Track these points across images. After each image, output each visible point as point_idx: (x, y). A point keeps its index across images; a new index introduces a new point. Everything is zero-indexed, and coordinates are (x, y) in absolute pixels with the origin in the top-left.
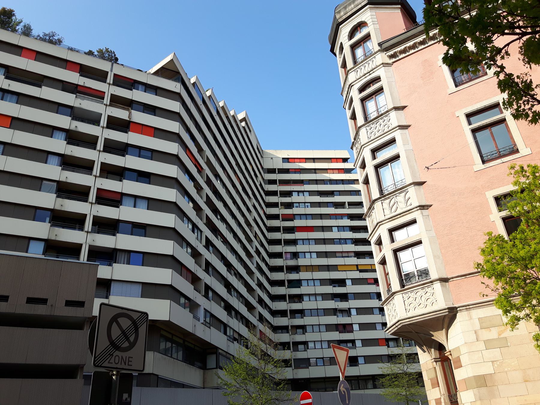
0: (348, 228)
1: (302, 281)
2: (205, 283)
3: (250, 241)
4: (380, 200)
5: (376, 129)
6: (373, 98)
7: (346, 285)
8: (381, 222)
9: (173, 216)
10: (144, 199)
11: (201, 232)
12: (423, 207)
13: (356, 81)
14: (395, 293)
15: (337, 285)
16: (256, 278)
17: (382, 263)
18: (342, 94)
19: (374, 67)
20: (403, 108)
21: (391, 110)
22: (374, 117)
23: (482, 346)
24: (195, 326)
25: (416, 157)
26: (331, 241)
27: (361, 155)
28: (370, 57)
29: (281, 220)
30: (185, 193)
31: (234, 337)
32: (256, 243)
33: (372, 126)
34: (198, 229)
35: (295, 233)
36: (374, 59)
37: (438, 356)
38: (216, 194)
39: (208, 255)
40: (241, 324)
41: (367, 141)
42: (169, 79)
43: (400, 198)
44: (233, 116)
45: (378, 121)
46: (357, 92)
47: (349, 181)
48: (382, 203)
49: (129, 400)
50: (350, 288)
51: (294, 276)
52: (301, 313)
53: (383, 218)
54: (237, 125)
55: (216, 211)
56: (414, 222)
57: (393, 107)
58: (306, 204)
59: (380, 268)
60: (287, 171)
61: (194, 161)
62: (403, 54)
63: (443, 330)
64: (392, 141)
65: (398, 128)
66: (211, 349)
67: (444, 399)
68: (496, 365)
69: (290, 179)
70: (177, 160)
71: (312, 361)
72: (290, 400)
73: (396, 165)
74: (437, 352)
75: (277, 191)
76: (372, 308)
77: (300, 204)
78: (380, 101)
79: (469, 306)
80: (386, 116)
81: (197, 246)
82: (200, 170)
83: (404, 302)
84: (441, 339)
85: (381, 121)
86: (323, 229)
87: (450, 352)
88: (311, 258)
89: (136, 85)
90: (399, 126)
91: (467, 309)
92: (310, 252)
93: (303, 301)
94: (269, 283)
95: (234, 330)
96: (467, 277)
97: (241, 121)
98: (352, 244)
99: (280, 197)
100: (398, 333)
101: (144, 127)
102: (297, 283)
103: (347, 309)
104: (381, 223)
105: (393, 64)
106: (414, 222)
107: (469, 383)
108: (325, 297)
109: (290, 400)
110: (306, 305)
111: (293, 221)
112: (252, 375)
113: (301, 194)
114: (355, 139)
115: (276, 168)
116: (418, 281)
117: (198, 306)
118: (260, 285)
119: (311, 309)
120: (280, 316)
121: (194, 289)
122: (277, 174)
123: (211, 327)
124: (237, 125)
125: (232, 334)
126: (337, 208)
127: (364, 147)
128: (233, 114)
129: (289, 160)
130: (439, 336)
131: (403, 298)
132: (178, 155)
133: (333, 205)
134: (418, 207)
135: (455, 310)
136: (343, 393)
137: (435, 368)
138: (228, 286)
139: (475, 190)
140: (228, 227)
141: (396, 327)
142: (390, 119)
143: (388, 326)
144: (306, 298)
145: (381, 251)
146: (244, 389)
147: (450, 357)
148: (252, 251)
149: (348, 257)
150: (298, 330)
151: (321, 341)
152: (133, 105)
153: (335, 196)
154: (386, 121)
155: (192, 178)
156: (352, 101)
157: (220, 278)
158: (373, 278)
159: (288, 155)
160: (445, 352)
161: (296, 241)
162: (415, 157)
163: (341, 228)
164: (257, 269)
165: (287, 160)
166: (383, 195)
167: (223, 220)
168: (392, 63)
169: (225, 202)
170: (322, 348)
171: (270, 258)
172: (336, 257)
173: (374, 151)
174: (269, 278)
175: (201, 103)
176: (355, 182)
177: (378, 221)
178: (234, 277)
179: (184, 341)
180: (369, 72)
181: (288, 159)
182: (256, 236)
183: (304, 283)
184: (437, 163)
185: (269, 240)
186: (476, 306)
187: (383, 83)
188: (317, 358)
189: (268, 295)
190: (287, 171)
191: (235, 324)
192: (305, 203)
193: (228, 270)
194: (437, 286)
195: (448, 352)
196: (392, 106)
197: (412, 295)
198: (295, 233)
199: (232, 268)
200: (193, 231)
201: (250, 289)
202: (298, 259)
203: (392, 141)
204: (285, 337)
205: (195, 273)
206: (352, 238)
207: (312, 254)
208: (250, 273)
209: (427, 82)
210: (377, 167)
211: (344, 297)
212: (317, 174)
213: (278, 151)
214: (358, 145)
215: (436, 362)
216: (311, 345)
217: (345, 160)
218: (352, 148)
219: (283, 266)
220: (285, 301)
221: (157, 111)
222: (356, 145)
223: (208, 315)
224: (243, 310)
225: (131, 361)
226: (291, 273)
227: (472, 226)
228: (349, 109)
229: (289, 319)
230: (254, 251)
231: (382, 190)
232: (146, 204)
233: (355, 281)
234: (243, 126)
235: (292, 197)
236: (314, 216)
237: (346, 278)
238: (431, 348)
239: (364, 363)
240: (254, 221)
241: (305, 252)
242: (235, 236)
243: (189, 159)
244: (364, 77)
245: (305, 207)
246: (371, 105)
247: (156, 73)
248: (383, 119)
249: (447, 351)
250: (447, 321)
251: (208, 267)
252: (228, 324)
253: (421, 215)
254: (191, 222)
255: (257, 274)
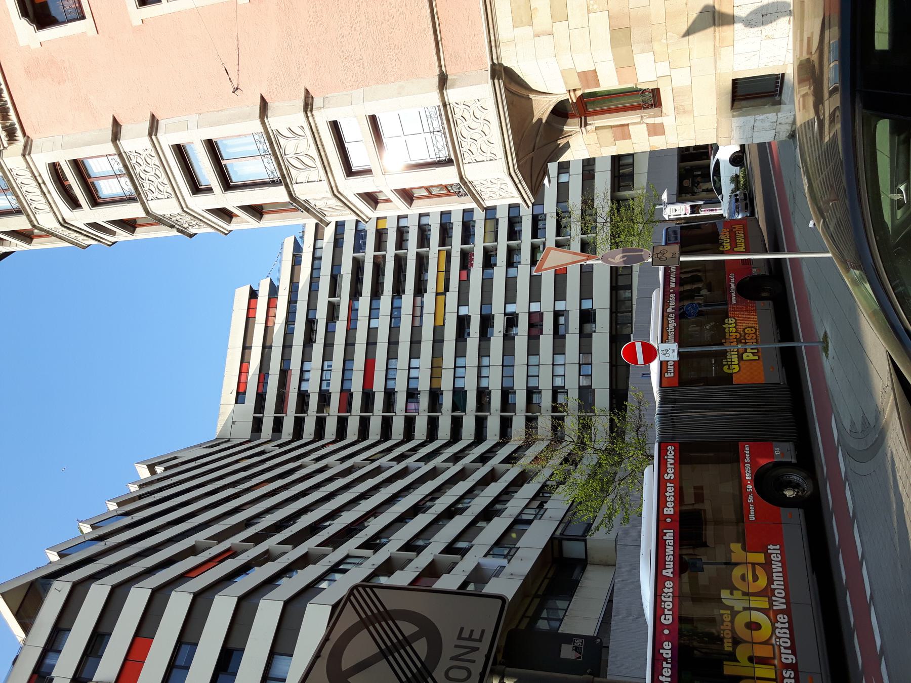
0: (374, 302)
1: (456, 386)
2: (441, 553)
3: (378, 471)
4: (290, 185)
5: (153, 182)
6: (93, 183)
7: (468, 315)
8: (332, 188)
9: (309, 606)
10: (272, 662)
11: (348, 556)
12: (308, 105)
13: (54, 213)
14: (461, 178)
15: (467, 330)
16: (444, 463)
17: (410, 201)
18: (84, 248)
19: (30, 175)
20: (116, 125)
21: (117, 147)
22: (129, 183)
23: (560, 27)
24: (512, 574)
25: (214, 110)
26: (394, 331)
27: (203, 217)
28: (9, 180)
29: (349, 414)
30: (270, 582)
31: (538, 507)
32: (384, 461)
33: (146, 189)
34: (341, 562)
35: (374, 391)
36: (14, 173)
37: (577, 120)
38: (284, 526)
39: (392, 547)
40: (516, 495)
41: (174, 200)
42: (43, 602)
43: (289, 147)
44: (141, 486)
45: (138, 176)
46: (77, 213)
47: (291, 292)
48: (297, 183)
49: (578, 642)
50: (473, 310)
51: (447, 400)
52: (507, 393)
53: (325, 183)
54: (159, 480)
55: (314, 529)
56: (335, 126)
57: (111, 143)
58: (324, 369)
59: (418, 205)
60: (261, 398)
61: (212, 564)
62: (9, 114)
63: (531, 97)
64: (180, 151)
65: (154, 137)
66: (554, 545)
67: (648, 118)
68: (595, 7)
69: (276, 392)
70: (203, 595)
71: (584, 382)
72: (639, 405)
73: (227, 150)
74: (570, 121)
75: (295, 416)
76: (506, 277)
77: (324, 378)
78: (100, 170)
79: (490, 42)
80: (129, 159)
81: (374, 565)
82: (231, 553)
83: (477, 162)
84: (546, 104)
85: (138, 170)
86: (371, 343)
87: (570, 91)
88: (419, 368)
89: (43, 669)
90: (150, 134)
91: (496, 46)
92: (409, 368)
93: (488, 387)
94: (455, 444)
95: (526, 507)
96: (439, 39)
97: (153, 472)
98: (401, 298)
99: (307, 413)
100: (533, 185)
101: (131, 657)
102: (459, 395)
103: (506, 317)
104: (334, 189)
105: (28, 137)
106: (335, 126)
107: (624, 64)
108: (484, 351)
109: (639, 405)
110: (494, 384)
111: (352, 393)
112: (596, 470)
113: (306, 376)
114: (172, 227)
115: (252, 417)
116: (442, 132)
117: (478, 567)
118: (456, 458)
119: (503, 377)
120: (509, 430)
121: (449, 573)
122: (263, 416)
123: (517, 546)
124: (159, 480)
125: (533, 512)
126: (338, 317)
127: (187, 207)
128: (137, 486)
129: (240, 391)
130: (542, 108)
131: (471, 163)
132: (194, 593)
133: (330, 323)
134: (306, 114)
135: (497, 68)
136: (625, 258)
137: (597, 128)
138: (450, 513)
139: (283, 6)
140: (347, 508)
141: (520, 182)
142: (136, 152)
143: (519, 200)
144: (484, 383)
145: (389, 201)
146: (619, 484)
147: (579, 93)
148: (397, 467)
149: (422, 307)
150: (535, 401)
151: (553, 365)
152: (83, 678)
153: (317, 318)
154: (139, 161)
155: (244, 569)
156: (95, 226)
157: (435, 527)
158: (460, 270)
159: (231, 393)
160: (571, 102)
161: (388, 391)
162: (213, 111)
163: (373, 313)
164: (428, 462)
165: (240, 396)
166: (283, 180)
167: (334, 515)
168: (26, 137)
169: (300, 510)
170: (564, 365)
171: (413, 439)
172: (421, 326)
173: (196, 188)
174: (447, 443)
175: (102, 543)
176: (294, 281)
177: (330, 195)
178: (438, 501)
179: (536, 596)
180: (39, 184)
181: (238, 393)
182: (371, 460)
183: (459, 383)
184: (226, 70)
185: (381, 438)
186: (492, 29)
187: (63, 159)
188: (580, 375)
189: (474, 447)
190: (261, 398)
191: (515, 506)
192: (322, 370)
193: (424, 512)
194: (452, 95)
195: (570, 94)
196: (111, 145)
197: (466, 145)
198: (375, 392)
199: (421, 504)
200: (344, 571)
201: (462, 475)
202: (419, 390)
203: (180, 151)
204: (544, 423)
205: (421, 570)
206: (391, 296)
207: (412, 365)
208: (433, 474)
209: (70, 73)
210: (227, 185)
211: (487, 321)
212: (273, 345)
213: (221, 411)
214: (185, 220)
215: (586, 124)
216: (558, 382)
217: (253, 294)
218: (191, 236)
219: (429, 416)
220: (485, 418)
221: (102, 630)
222: (185, 226)
223: (497, 550)
224: (495, 489)
225: (472, 631)
226: (442, 404)
227: (349, 18)
228: (113, 233)
229: (515, 415)
230: (398, 464)
231: (273, 181)
232: (282, 659)
233: (463, 299)
234: (164, 471)
235: (309, 392)
236: (348, 357)
237: (456, 313)
238: (562, 130)
239: (591, 300)
240: (343, 462)
241: (409, 378)
242: (364, 496)
243: (208, 571)
244: (48, 196)
245: (331, 370)
246: (107, 189)
247: (26, 627)
248: (135, 165)
249: (568, 97)
250: (514, 88)
251: (411, 546)
252: (515, 517)
253: (322, 110)
254: (327, 575)
255: (437, 461)
